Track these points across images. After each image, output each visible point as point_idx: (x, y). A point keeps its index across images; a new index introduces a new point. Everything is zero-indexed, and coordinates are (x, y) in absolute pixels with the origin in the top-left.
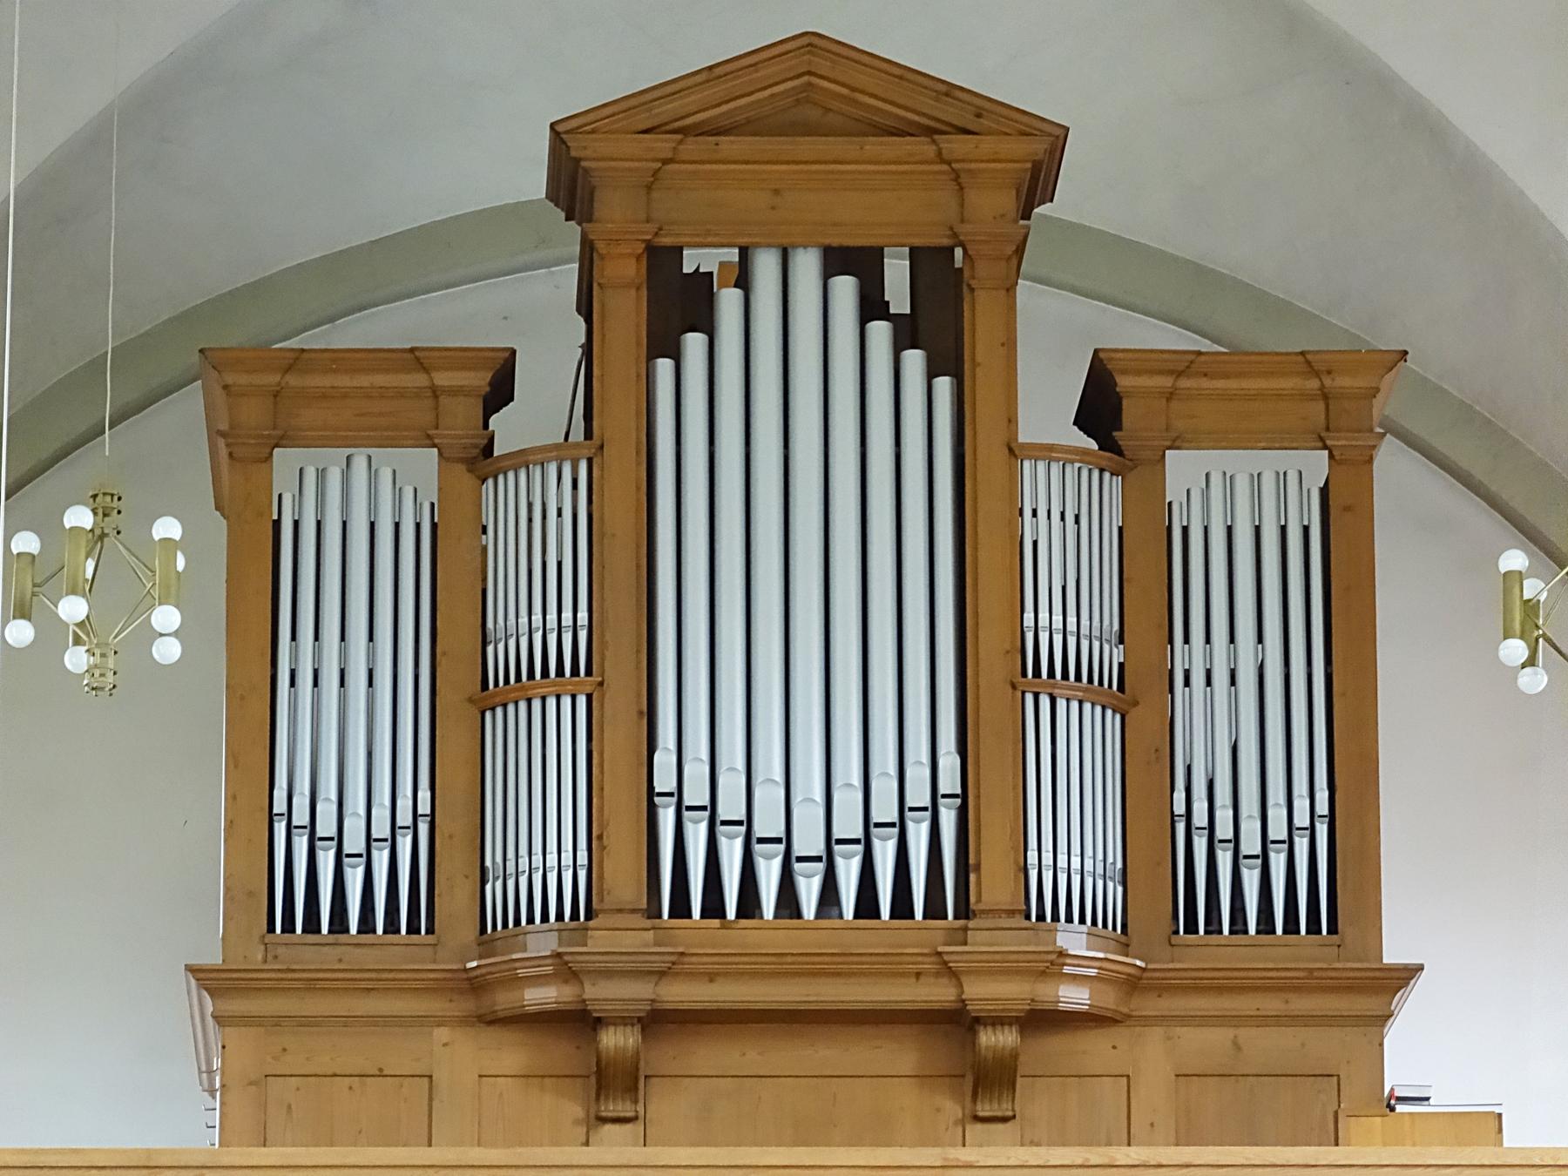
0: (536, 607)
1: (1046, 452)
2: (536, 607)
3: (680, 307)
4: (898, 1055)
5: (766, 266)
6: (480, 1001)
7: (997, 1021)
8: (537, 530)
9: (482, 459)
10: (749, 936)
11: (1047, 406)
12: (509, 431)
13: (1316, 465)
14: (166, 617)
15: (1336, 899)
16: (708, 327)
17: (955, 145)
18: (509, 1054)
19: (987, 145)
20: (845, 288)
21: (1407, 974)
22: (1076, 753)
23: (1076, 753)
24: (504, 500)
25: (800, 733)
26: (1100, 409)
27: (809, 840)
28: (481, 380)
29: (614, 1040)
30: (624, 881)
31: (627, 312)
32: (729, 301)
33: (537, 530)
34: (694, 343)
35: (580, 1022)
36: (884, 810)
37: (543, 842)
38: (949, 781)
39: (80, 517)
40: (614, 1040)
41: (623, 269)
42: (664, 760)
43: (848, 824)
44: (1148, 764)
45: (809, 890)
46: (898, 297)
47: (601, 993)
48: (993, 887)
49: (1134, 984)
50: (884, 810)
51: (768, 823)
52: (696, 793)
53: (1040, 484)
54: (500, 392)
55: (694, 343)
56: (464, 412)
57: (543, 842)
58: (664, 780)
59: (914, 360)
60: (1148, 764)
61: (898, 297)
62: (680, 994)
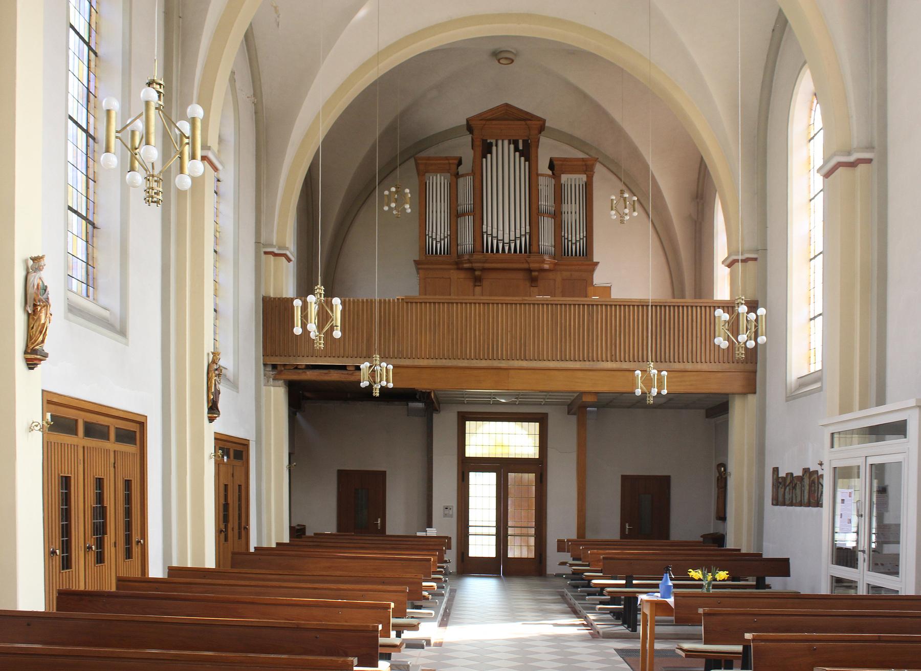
0: (466, 201)
1: (542, 175)
2: (466, 201)
3: (487, 149)
4: (521, 275)
5: (500, 142)
6: (458, 265)
7: (535, 271)
8: (466, 185)
9: (457, 175)
10: (498, 256)
11: (543, 166)
12: (461, 170)
13: (584, 178)
14: (407, 206)
15: (588, 251)
16: (491, 153)
17: (529, 122)
18: (462, 275)
19: (533, 122)
20: (512, 146)
21: (598, 263)
22: (547, 226)
23: (547, 226)
24: (461, 180)
25: (505, 225)
26: (551, 166)
27: (506, 241)
28: (456, 162)
29: (477, 273)
30: (479, 248)
31: (479, 150)
32: (494, 148)
33: (466, 185)
34: (489, 156)
35: (472, 270)
36: (518, 235)
37: (467, 241)
38: (528, 231)
39: (393, 189)
40: (477, 273)
41: (478, 143)
42: (485, 227)
43: (512, 238)
44: (559, 227)
45: (507, 248)
46: (521, 148)
47: (476, 265)
48: (534, 249)
49: (555, 264)
50: (518, 235)
51: (500, 237)
52: (489, 232)
53: (542, 180)
54: (460, 163)
55: (489, 156)
56: (454, 167)
57: (467, 241)
58: (485, 230)
59: (523, 159)
60: (559, 227)
61: (521, 148)
62: (487, 265)
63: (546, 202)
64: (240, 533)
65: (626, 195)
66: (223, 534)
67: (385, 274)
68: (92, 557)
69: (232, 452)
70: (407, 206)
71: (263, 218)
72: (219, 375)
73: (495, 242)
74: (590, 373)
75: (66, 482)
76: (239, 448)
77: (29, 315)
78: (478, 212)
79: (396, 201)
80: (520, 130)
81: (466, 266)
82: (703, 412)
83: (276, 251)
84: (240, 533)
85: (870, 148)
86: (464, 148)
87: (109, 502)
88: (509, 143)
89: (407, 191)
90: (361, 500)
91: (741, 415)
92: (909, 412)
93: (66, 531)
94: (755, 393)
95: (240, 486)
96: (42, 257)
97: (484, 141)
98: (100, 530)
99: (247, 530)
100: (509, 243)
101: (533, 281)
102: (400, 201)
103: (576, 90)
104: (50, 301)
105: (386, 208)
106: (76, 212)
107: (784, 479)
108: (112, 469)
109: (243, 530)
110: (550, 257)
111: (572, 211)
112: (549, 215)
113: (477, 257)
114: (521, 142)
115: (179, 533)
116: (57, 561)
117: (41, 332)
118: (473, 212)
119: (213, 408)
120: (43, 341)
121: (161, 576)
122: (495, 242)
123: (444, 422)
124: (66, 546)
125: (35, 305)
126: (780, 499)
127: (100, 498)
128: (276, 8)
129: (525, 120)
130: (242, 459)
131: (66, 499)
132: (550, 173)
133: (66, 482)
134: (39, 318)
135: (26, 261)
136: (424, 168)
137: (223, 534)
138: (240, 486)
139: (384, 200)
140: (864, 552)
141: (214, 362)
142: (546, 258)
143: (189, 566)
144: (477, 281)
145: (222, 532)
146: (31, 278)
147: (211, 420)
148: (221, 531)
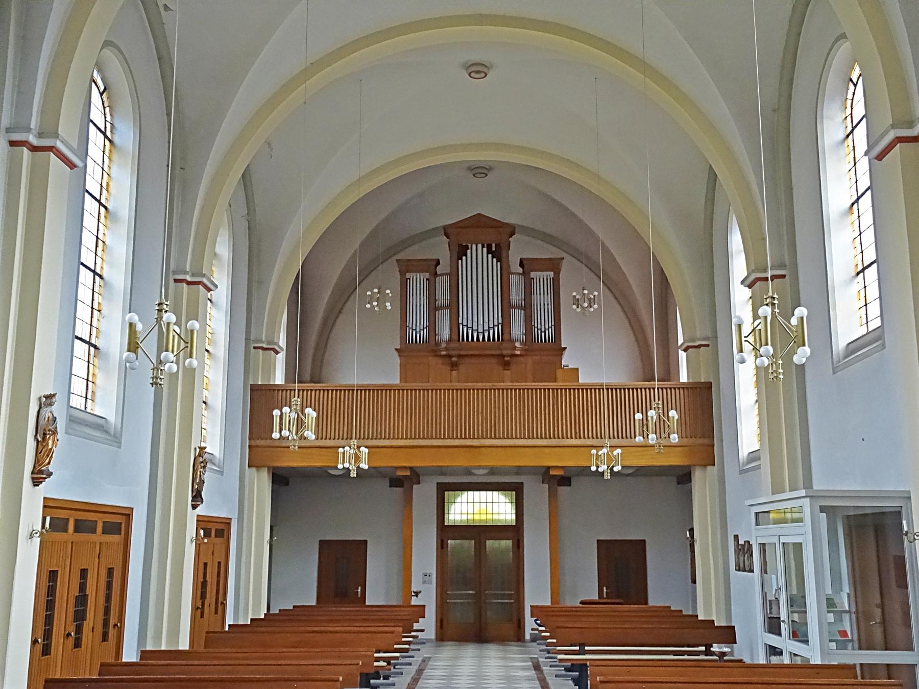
0: (443, 297)
3: (462, 251)
4: (494, 361)
5: (474, 246)
6: (435, 353)
8: (443, 285)
9: (436, 274)
12: (439, 270)
14: (388, 304)
16: (466, 255)
18: (440, 361)
22: (517, 316)
23: (517, 316)
24: (438, 279)
25: (480, 317)
26: (522, 265)
27: (481, 330)
28: (435, 263)
29: (454, 359)
32: (469, 251)
33: (443, 285)
34: (464, 258)
36: (491, 326)
38: (500, 321)
42: (460, 319)
44: (528, 319)
48: (506, 337)
49: (526, 350)
52: (465, 323)
53: (513, 278)
54: (438, 263)
58: (460, 321)
62: (463, 353)
63: (516, 296)
64: (216, 609)
65: (586, 292)
66: (199, 611)
67: (367, 362)
68: (71, 642)
69: (215, 531)
70: (388, 304)
71: (255, 295)
72: (204, 467)
73: (470, 332)
74: (558, 449)
75: (53, 575)
76: (220, 527)
77: (38, 441)
78: (454, 304)
79: (378, 300)
80: (494, 236)
81: (444, 353)
82: (675, 479)
83: (265, 346)
84: (216, 609)
85: (782, 266)
86: (441, 250)
87: (90, 590)
88: (483, 247)
89: (388, 291)
90: (342, 568)
91: (702, 483)
92: (803, 500)
93: (49, 620)
94: (714, 465)
95: (219, 563)
96: (54, 395)
97: (460, 246)
98: (80, 616)
99: (224, 605)
100: (483, 333)
101: (506, 365)
102: (381, 304)
103: (548, 197)
104: (58, 430)
105: (368, 306)
106: (81, 339)
107: (743, 546)
108: (97, 560)
109: (220, 605)
110: (521, 344)
111: (542, 299)
112: (520, 308)
113: (452, 345)
114: (494, 245)
115: (157, 618)
116: (39, 648)
117: (48, 456)
118: (449, 307)
119: (197, 497)
120: (49, 463)
121: (134, 660)
122: (470, 332)
123: (424, 492)
124: (48, 635)
125: (45, 434)
126: (742, 565)
127: (83, 587)
128: (269, 144)
129: (496, 227)
130: (223, 537)
131: (51, 591)
132: (521, 270)
133: (53, 575)
134: (48, 444)
135: (40, 399)
136: (406, 267)
137: (199, 611)
138: (219, 563)
139: (364, 300)
140: (784, 621)
141: (200, 455)
142: (517, 344)
143: (163, 648)
144: (454, 366)
145: (198, 610)
146: (43, 412)
147: (194, 507)
148: (198, 608)
